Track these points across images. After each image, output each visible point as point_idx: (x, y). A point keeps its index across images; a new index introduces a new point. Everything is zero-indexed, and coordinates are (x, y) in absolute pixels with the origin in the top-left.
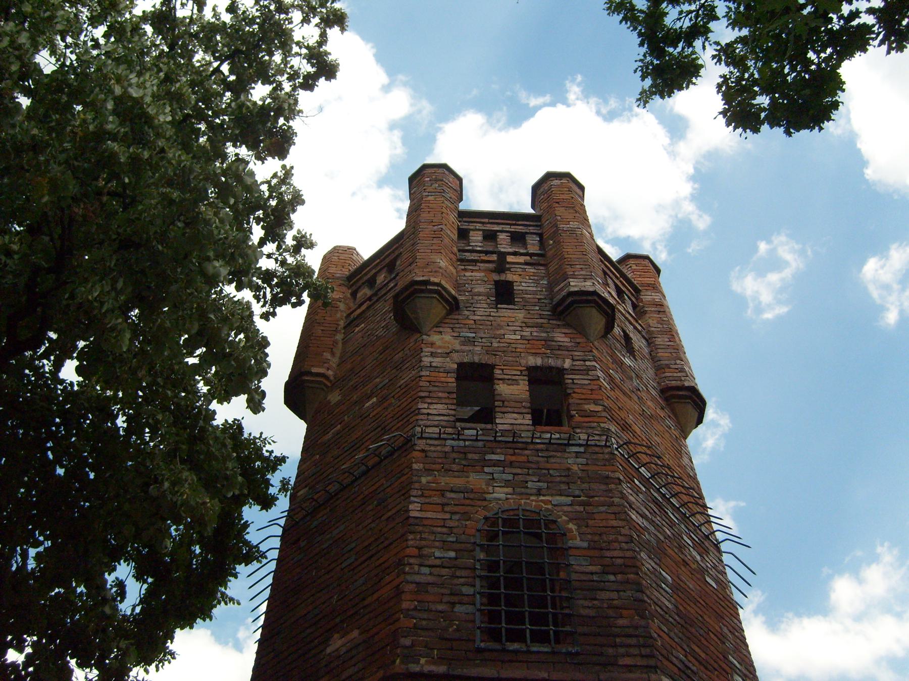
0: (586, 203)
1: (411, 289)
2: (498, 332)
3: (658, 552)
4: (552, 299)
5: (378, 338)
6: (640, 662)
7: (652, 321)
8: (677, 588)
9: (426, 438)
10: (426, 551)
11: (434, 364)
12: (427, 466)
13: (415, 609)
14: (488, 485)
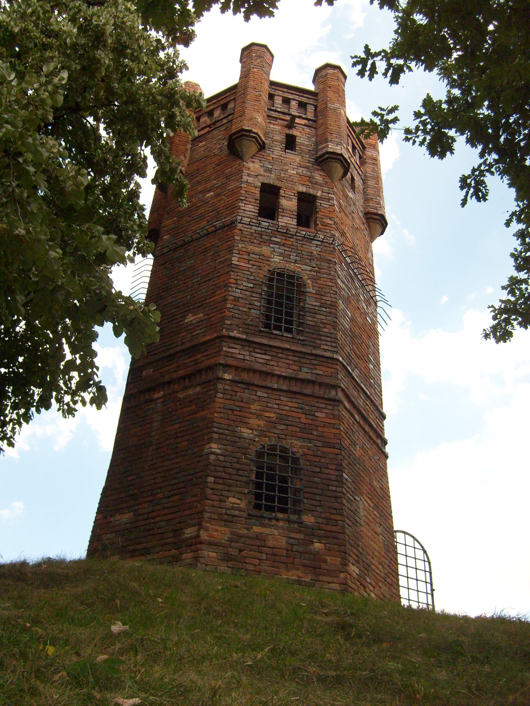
0: (346, 89)
1: (241, 133)
2: (285, 167)
3: (347, 301)
4: (317, 152)
5: (215, 155)
6: (330, 348)
7: (368, 168)
8: (352, 320)
9: (242, 223)
10: (239, 282)
11: (249, 181)
12: (243, 239)
13: (233, 308)
14: (271, 253)
